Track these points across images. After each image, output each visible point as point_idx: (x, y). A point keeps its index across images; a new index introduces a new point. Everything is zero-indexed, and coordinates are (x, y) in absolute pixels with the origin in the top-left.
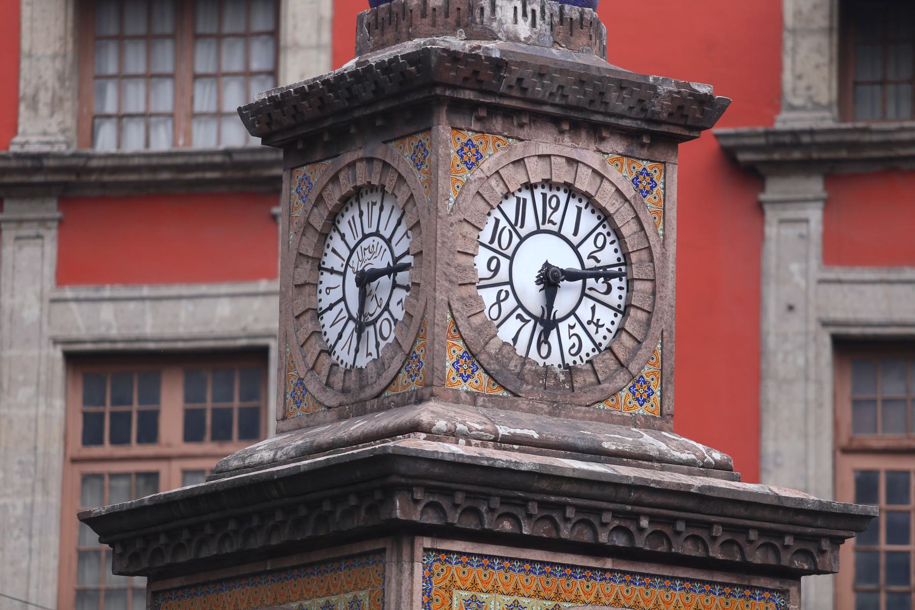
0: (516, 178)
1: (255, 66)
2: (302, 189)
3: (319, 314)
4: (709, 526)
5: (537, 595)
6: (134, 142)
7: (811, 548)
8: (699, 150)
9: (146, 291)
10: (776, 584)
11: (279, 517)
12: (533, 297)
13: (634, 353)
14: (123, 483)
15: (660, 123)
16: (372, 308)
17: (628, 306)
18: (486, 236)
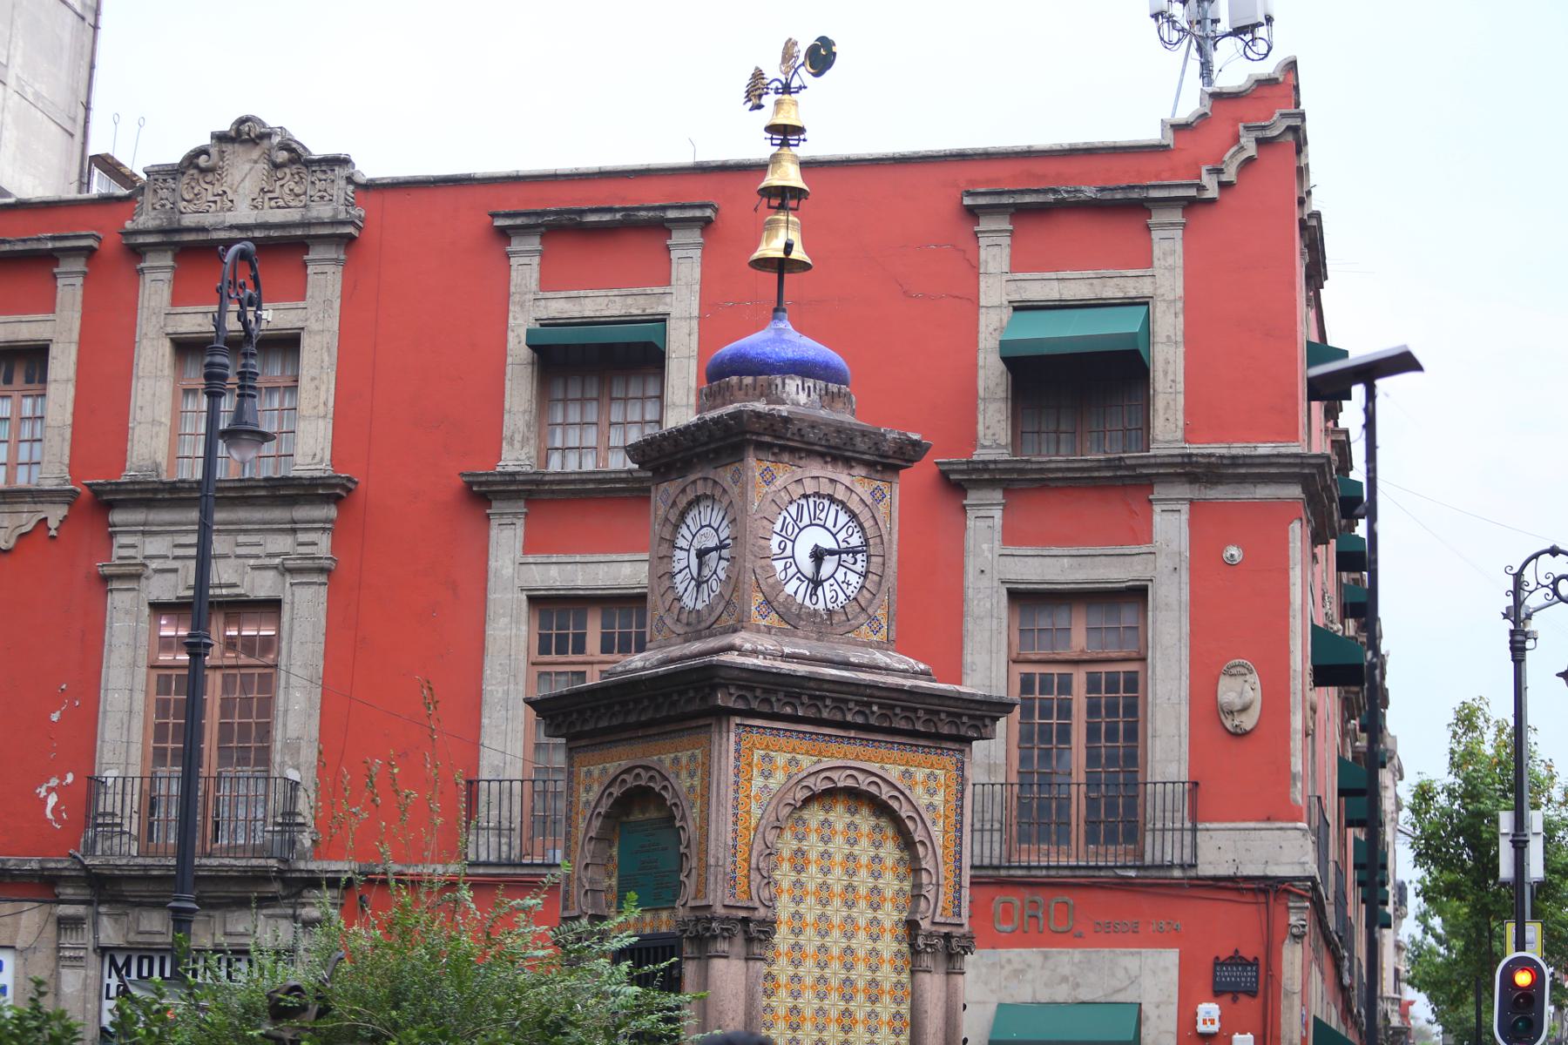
0: (797, 491)
1: (648, 418)
2: (664, 495)
3: (673, 576)
4: (915, 710)
5: (807, 753)
6: (572, 465)
7: (979, 723)
8: (921, 473)
9: (578, 558)
10: (957, 746)
11: (646, 703)
12: (807, 566)
13: (870, 602)
14: (563, 678)
15: (888, 457)
16: (706, 572)
17: (867, 572)
18: (777, 527)
